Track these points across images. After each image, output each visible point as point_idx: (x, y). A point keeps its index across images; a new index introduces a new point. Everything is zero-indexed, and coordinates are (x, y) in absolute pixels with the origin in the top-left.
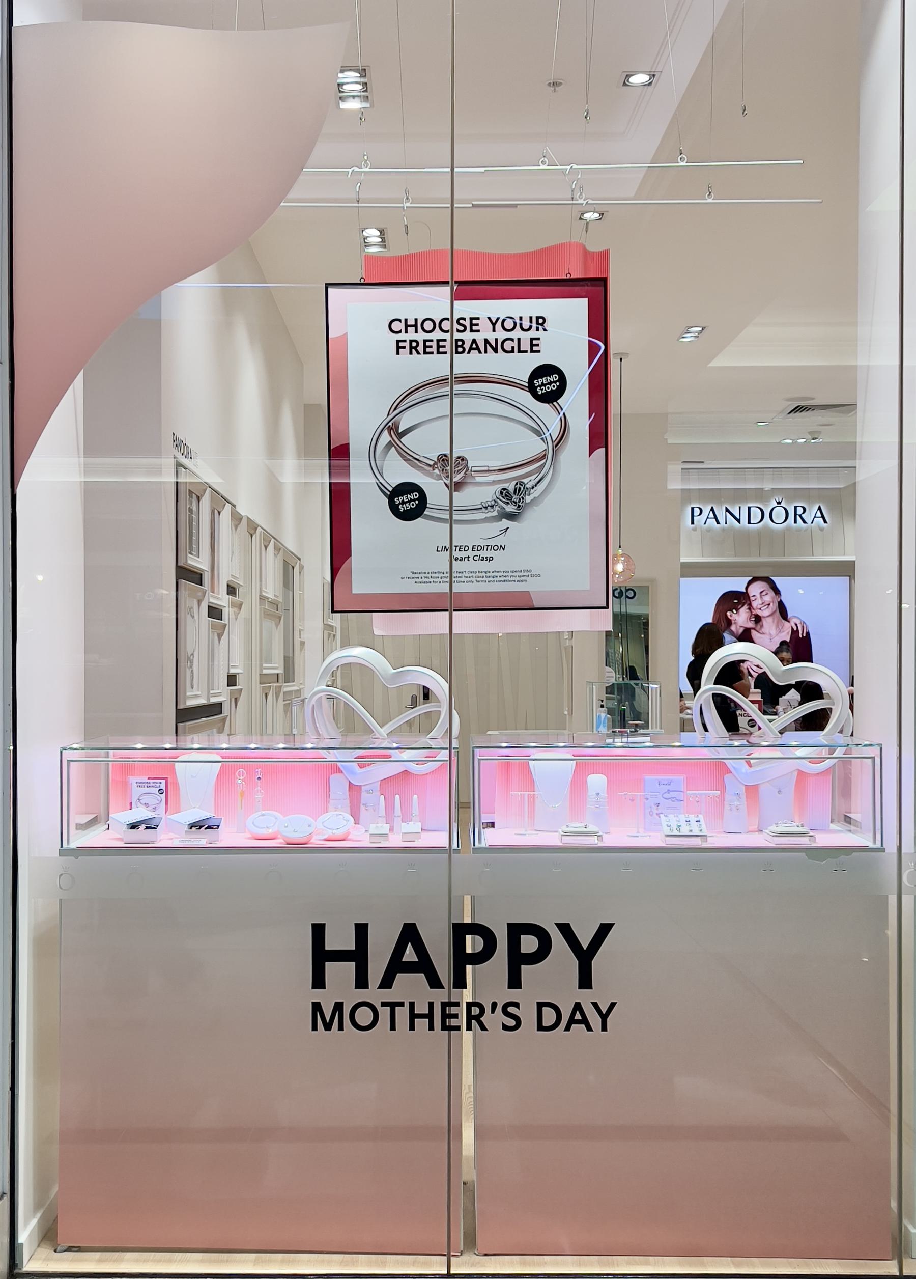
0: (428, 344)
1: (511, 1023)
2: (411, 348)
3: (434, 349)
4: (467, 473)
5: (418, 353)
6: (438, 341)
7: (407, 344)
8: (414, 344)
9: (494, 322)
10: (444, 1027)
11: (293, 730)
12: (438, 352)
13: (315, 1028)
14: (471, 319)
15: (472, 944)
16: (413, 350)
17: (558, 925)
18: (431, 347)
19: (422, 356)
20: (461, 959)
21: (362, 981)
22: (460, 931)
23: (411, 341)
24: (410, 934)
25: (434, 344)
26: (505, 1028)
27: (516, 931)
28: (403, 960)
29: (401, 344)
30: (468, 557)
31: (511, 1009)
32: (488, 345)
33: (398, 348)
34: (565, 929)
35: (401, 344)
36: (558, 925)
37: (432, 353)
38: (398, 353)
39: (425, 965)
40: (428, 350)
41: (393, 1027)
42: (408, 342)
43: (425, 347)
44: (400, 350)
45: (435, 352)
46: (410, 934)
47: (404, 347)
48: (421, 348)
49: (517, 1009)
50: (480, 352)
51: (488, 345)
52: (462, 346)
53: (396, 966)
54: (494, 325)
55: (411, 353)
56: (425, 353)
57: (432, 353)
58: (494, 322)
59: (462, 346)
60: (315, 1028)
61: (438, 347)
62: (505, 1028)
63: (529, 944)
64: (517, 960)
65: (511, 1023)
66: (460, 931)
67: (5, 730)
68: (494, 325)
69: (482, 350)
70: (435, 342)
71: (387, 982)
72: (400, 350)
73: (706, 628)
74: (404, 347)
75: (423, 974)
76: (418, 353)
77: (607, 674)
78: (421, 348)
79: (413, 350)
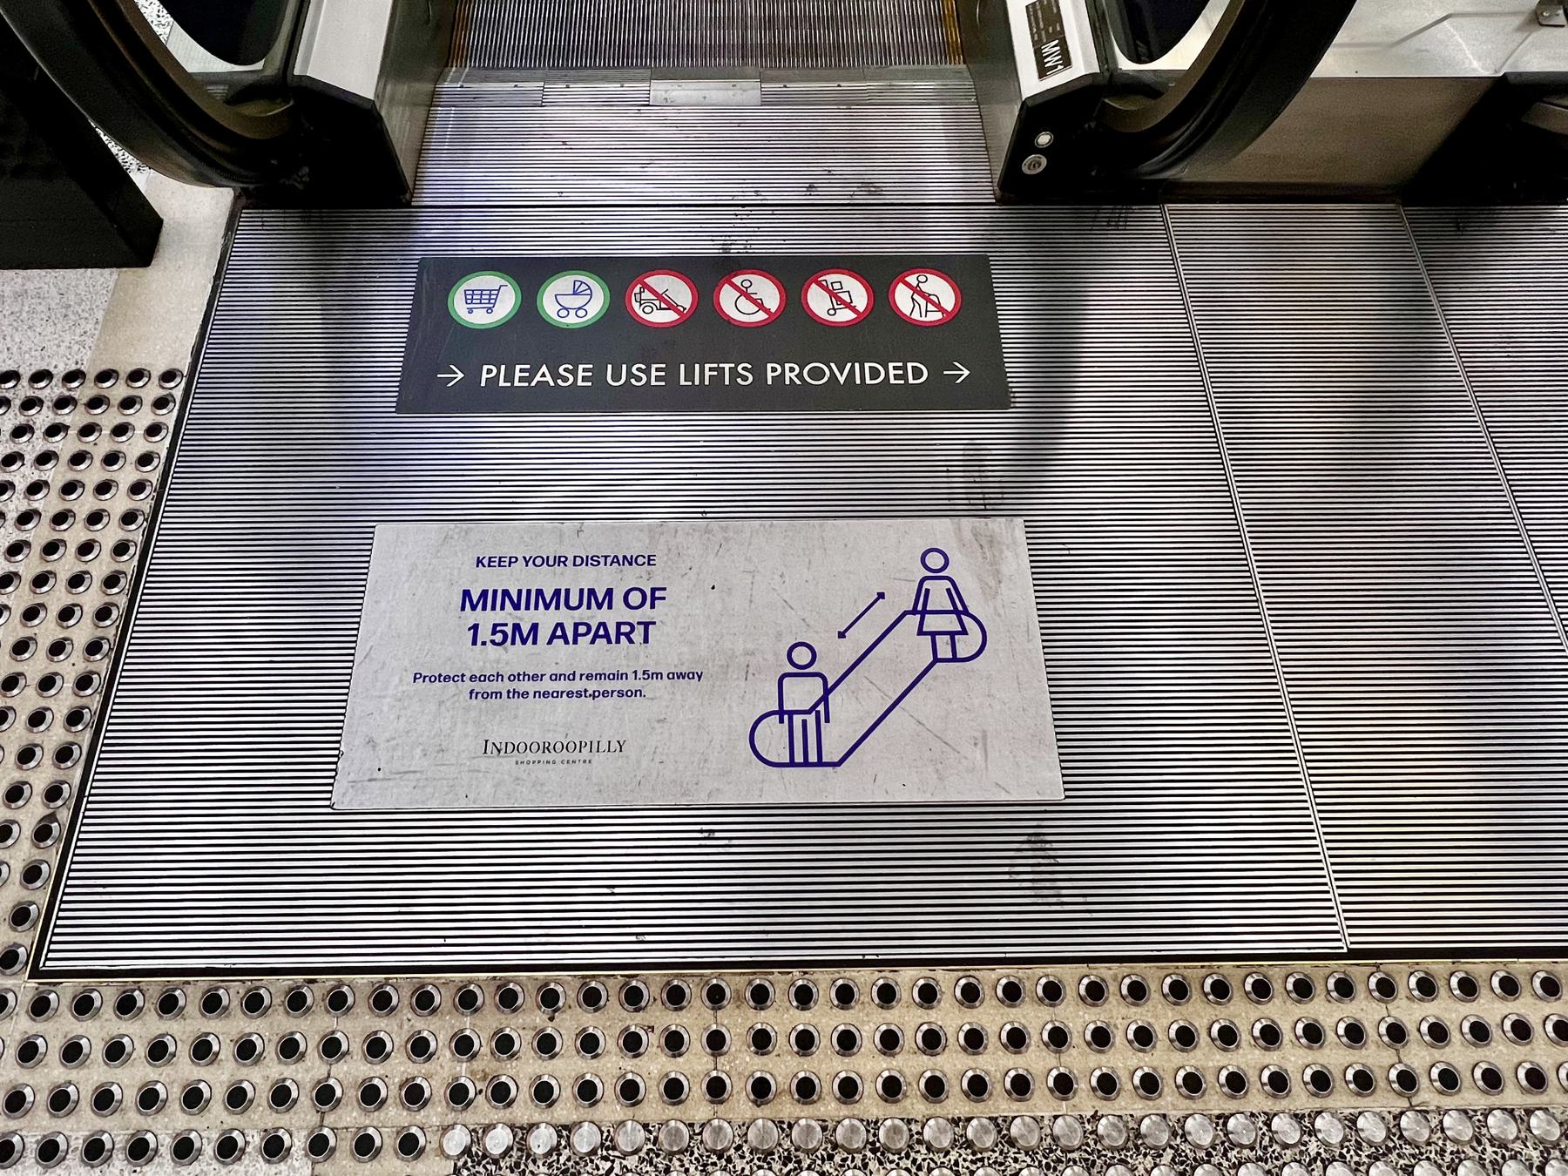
3: (496, 564)
5: (484, 566)
11: (584, 1149)
12: (500, 566)
13: (463, 608)
14: (490, 558)
19: (487, 568)
30: (463, 675)
32: (507, 599)
43: (490, 561)
50: (609, 642)
51: (507, 599)
54: (527, 562)
56: (489, 566)
60: (463, 608)
61: (500, 561)
67: (980, 745)
68: (527, 562)
69: (613, 638)
73: (354, 1114)
76: (484, 566)
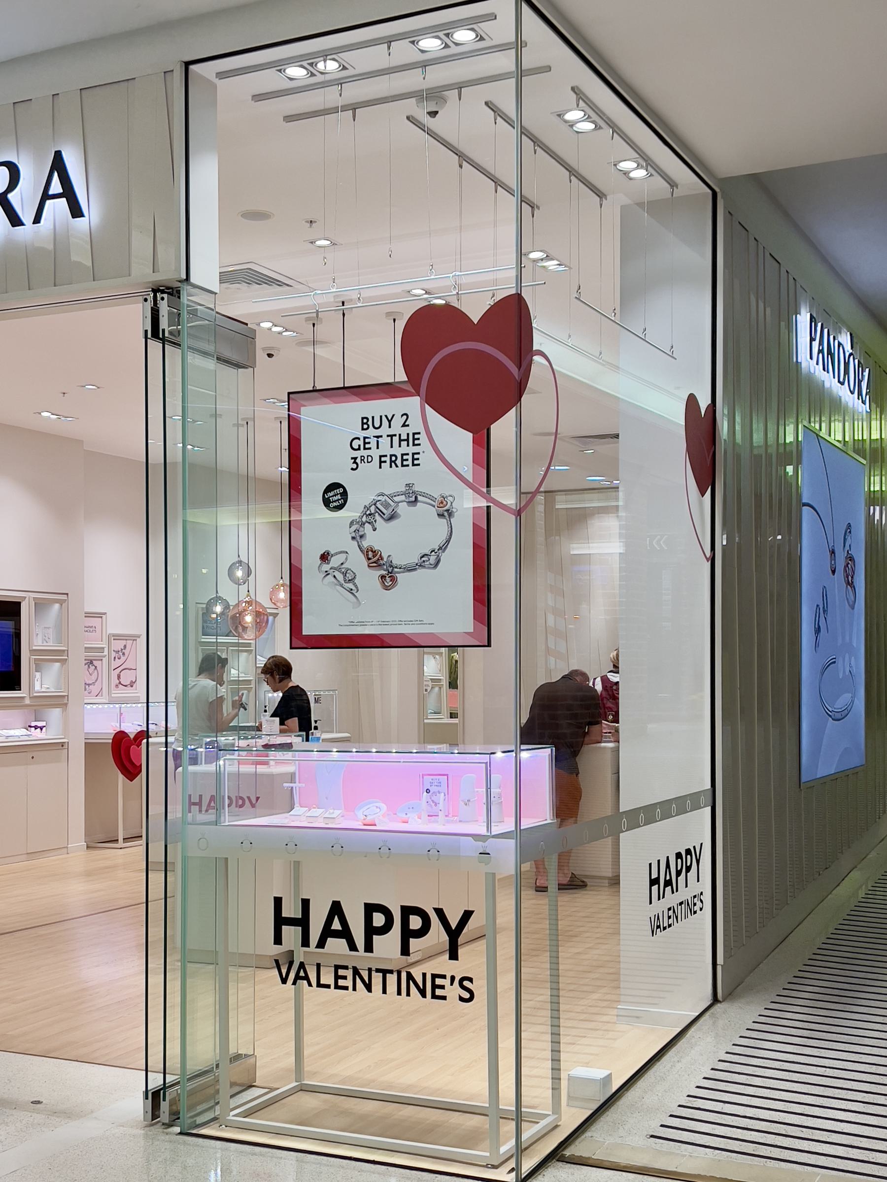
0: (405, 457)
1: (466, 995)
2: (391, 461)
3: (410, 462)
4: (615, 652)
6: (413, 454)
7: (387, 459)
8: (394, 458)
9: (51, 192)
10: (434, 996)
12: (414, 465)
15: (379, 920)
16: (393, 464)
17: (435, 909)
18: (407, 460)
20: (371, 931)
21: (305, 943)
22: (370, 909)
23: (391, 456)
24: (336, 909)
25: (410, 457)
26: (462, 999)
27: (407, 911)
28: (332, 928)
29: (383, 459)
31: (466, 983)
33: (381, 462)
34: (440, 912)
35: (383, 459)
36: (435, 909)
37: (408, 466)
38: (380, 467)
39: (345, 933)
40: (405, 463)
41: (384, 992)
42: (389, 456)
43: (403, 460)
44: (382, 464)
45: (411, 464)
46: (336, 909)
47: (385, 462)
48: (399, 462)
49: (471, 984)
52: (366, 423)
53: (327, 933)
55: (391, 467)
56: (403, 466)
57: (408, 466)
58: (51, 192)
59: (366, 423)
61: (414, 459)
62: (462, 999)
63: (415, 922)
64: (407, 934)
65: (466, 995)
66: (370, 909)
70: (411, 455)
71: (321, 944)
72: (382, 464)
74: (385, 462)
75: (345, 940)
76: (397, 466)
77: (425, 683)
78: (399, 462)
79: (393, 464)
